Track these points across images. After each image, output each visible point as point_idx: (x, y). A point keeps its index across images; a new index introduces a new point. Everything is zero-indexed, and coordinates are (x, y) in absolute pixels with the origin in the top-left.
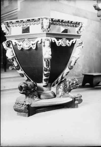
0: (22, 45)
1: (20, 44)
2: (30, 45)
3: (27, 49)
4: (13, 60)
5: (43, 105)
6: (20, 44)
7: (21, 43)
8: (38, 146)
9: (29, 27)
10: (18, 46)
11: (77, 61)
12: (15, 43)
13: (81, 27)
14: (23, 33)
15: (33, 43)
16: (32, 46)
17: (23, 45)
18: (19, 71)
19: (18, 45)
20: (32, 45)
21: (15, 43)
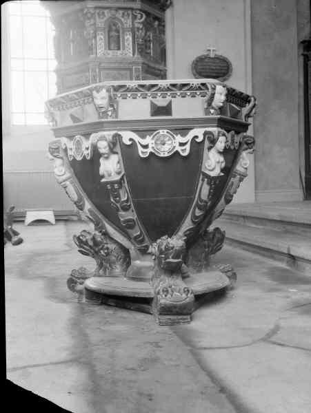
0: (150, 146)
1: (143, 144)
2: (174, 147)
3: (166, 155)
4: (121, 187)
5: (124, 292)
6: (144, 142)
7: (148, 140)
8: (120, 295)
9: (170, 104)
10: (140, 149)
11: (130, 366)
12: (131, 140)
13: (216, 296)
14: (152, 115)
15: (183, 140)
16: (179, 149)
17: (154, 145)
18: (225, 55)
19: (139, 146)
20: (182, 144)
21: (131, 140)
